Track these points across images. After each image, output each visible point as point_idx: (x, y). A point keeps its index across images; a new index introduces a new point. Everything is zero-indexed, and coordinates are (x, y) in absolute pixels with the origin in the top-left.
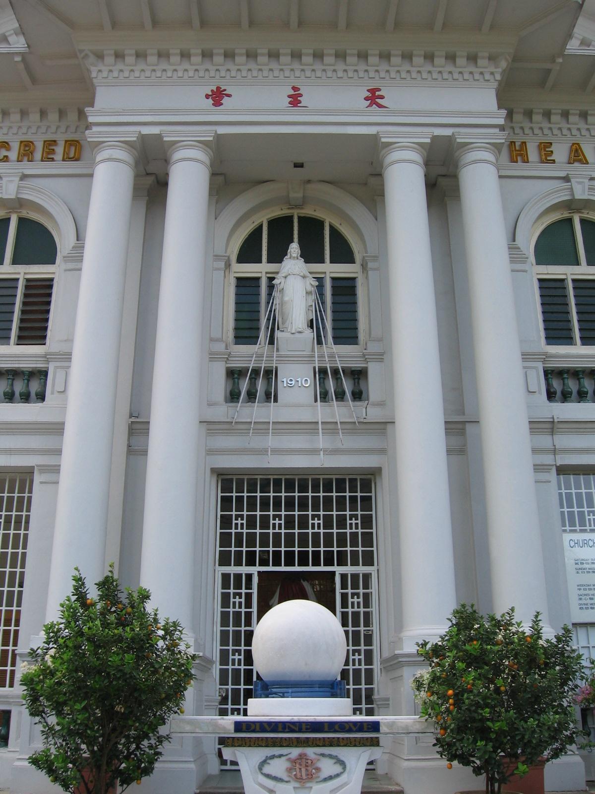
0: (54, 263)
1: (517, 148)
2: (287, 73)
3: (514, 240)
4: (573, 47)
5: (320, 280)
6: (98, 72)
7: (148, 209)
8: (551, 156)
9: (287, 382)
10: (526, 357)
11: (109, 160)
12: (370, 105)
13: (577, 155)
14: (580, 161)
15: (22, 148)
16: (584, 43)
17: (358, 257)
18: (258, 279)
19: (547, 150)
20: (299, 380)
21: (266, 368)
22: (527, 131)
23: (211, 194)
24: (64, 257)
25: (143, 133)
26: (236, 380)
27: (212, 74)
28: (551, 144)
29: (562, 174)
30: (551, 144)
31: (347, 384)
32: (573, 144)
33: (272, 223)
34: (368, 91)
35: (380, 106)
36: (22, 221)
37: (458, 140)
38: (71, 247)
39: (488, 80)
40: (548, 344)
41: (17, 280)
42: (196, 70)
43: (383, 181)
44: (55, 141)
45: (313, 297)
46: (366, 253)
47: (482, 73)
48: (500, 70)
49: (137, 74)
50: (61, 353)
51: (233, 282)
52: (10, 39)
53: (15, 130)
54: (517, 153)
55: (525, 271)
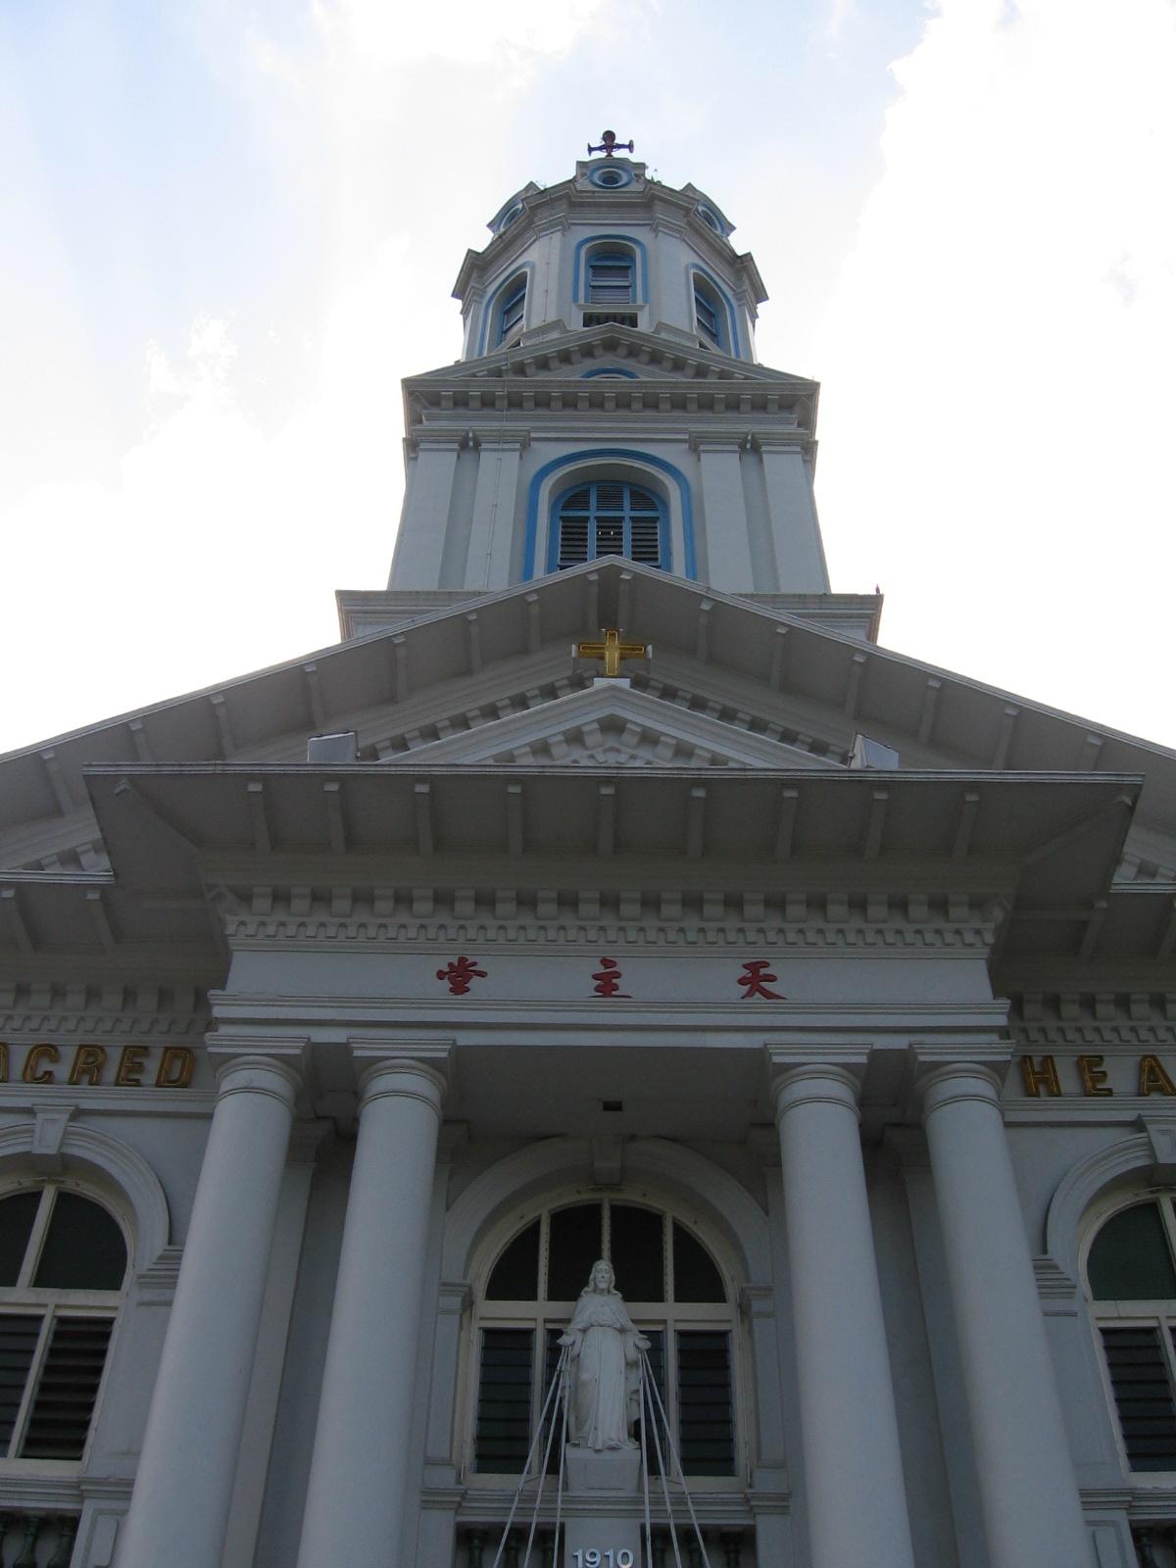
0: (118, 1288)
1: (1037, 1068)
2: (592, 934)
3: (1045, 1251)
4: (1124, 878)
5: (655, 1338)
6: (238, 926)
7: (314, 1186)
8: (1099, 1064)
9: (584, 1557)
10: (1090, 1499)
11: (247, 1089)
12: (749, 994)
13: (1152, 1079)
14: (1161, 1090)
15: (82, 1058)
16: (1145, 870)
17: (731, 1290)
18: (528, 1333)
19: (1095, 1070)
20: (610, 1553)
21: (553, 1212)
22: (1052, 1035)
23: (439, 1161)
24: (140, 1277)
25: (313, 1040)
26: (477, 1553)
27: (452, 933)
28: (1101, 1057)
29: (1129, 1116)
30: (1101, 1057)
32: (1145, 1057)
33: (560, 1219)
34: (745, 966)
35: (768, 995)
36: (64, 1199)
37: (922, 1058)
38: (154, 1260)
39: (971, 945)
40: (1135, 1468)
41: (39, 1319)
42: (423, 927)
43: (778, 1136)
44: (146, 1048)
45: (641, 1373)
46: (748, 1281)
47: (958, 932)
48: (992, 925)
49: (311, 931)
50: (112, 1480)
51: (476, 1339)
52: (84, 859)
53: (71, 1025)
54: (1037, 1078)
55: (1074, 1315)
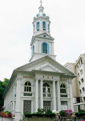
31: (50, 95)
